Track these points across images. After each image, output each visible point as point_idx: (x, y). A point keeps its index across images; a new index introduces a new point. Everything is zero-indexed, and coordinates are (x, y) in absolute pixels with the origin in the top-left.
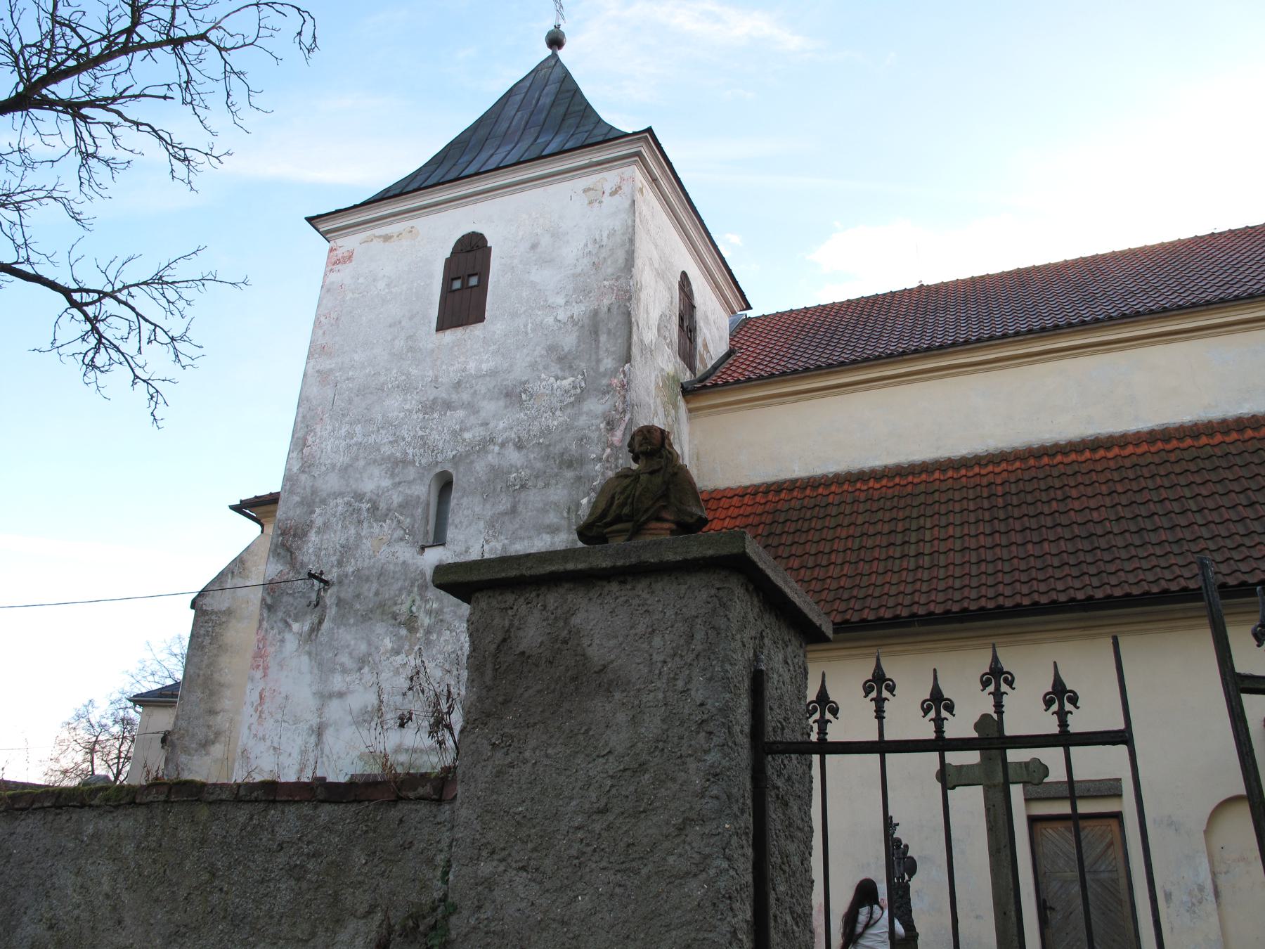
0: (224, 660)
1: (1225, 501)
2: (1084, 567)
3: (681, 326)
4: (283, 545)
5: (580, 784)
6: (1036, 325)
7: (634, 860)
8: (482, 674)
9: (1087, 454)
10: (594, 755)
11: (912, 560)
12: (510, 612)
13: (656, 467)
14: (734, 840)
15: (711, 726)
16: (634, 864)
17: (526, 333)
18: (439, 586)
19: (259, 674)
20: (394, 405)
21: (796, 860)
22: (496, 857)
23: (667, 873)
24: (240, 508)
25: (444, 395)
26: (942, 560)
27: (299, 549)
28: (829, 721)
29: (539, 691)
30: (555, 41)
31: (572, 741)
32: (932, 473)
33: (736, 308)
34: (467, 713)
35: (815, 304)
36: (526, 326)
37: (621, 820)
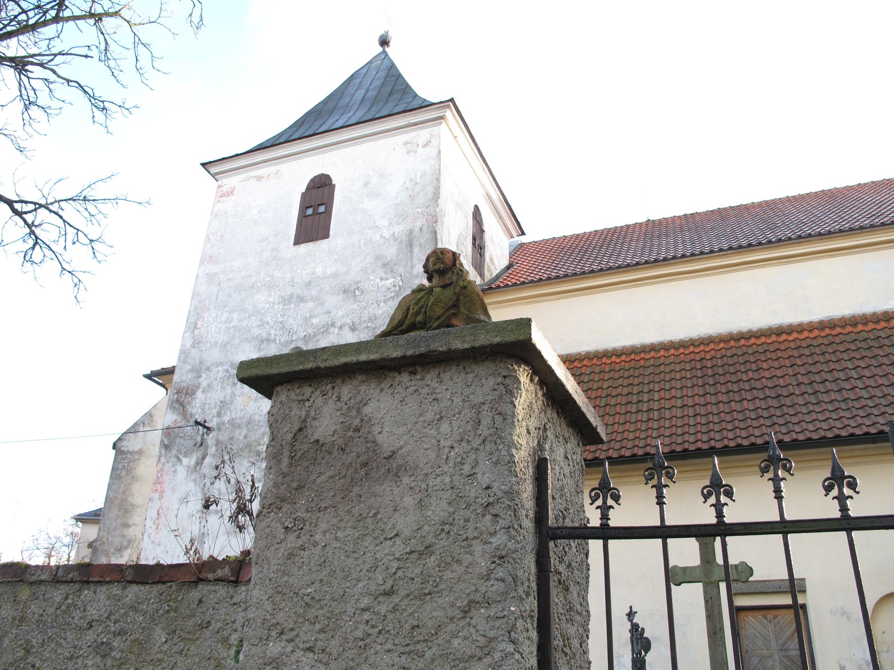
0: (136, 487)
1: (879, 371)
2: (775, 419)
3: (474, 244)
4: (178, 401)
5: (368, 566)
6: (735, 244)
7: (418, 642)
8: (279, 462)
9: (774, 338)
10: (382, 538)
11: (645, 414)
12: (307, 404)
13: (448, 282)
14: (520, 624)
15: (496, 510)
16: (419, 646)
17: (360, 246)
18: (243, 380)
19: (157, 496)
20: (261, 299)
21: (575, 643)
22: (284, 637)
23: (451, 657)
24: (149, 377)
25: (299, 292)
26: (667, 414)
27: (189, 403)
28: (611, 507)
29: (331, 477)
30: (384, 42)
31: (361, 524)
32: (659, 351)
33: (514, 234)
34: (264, 498)
35: (572, 234)
36: (359, 241)
37: (406, 601)
